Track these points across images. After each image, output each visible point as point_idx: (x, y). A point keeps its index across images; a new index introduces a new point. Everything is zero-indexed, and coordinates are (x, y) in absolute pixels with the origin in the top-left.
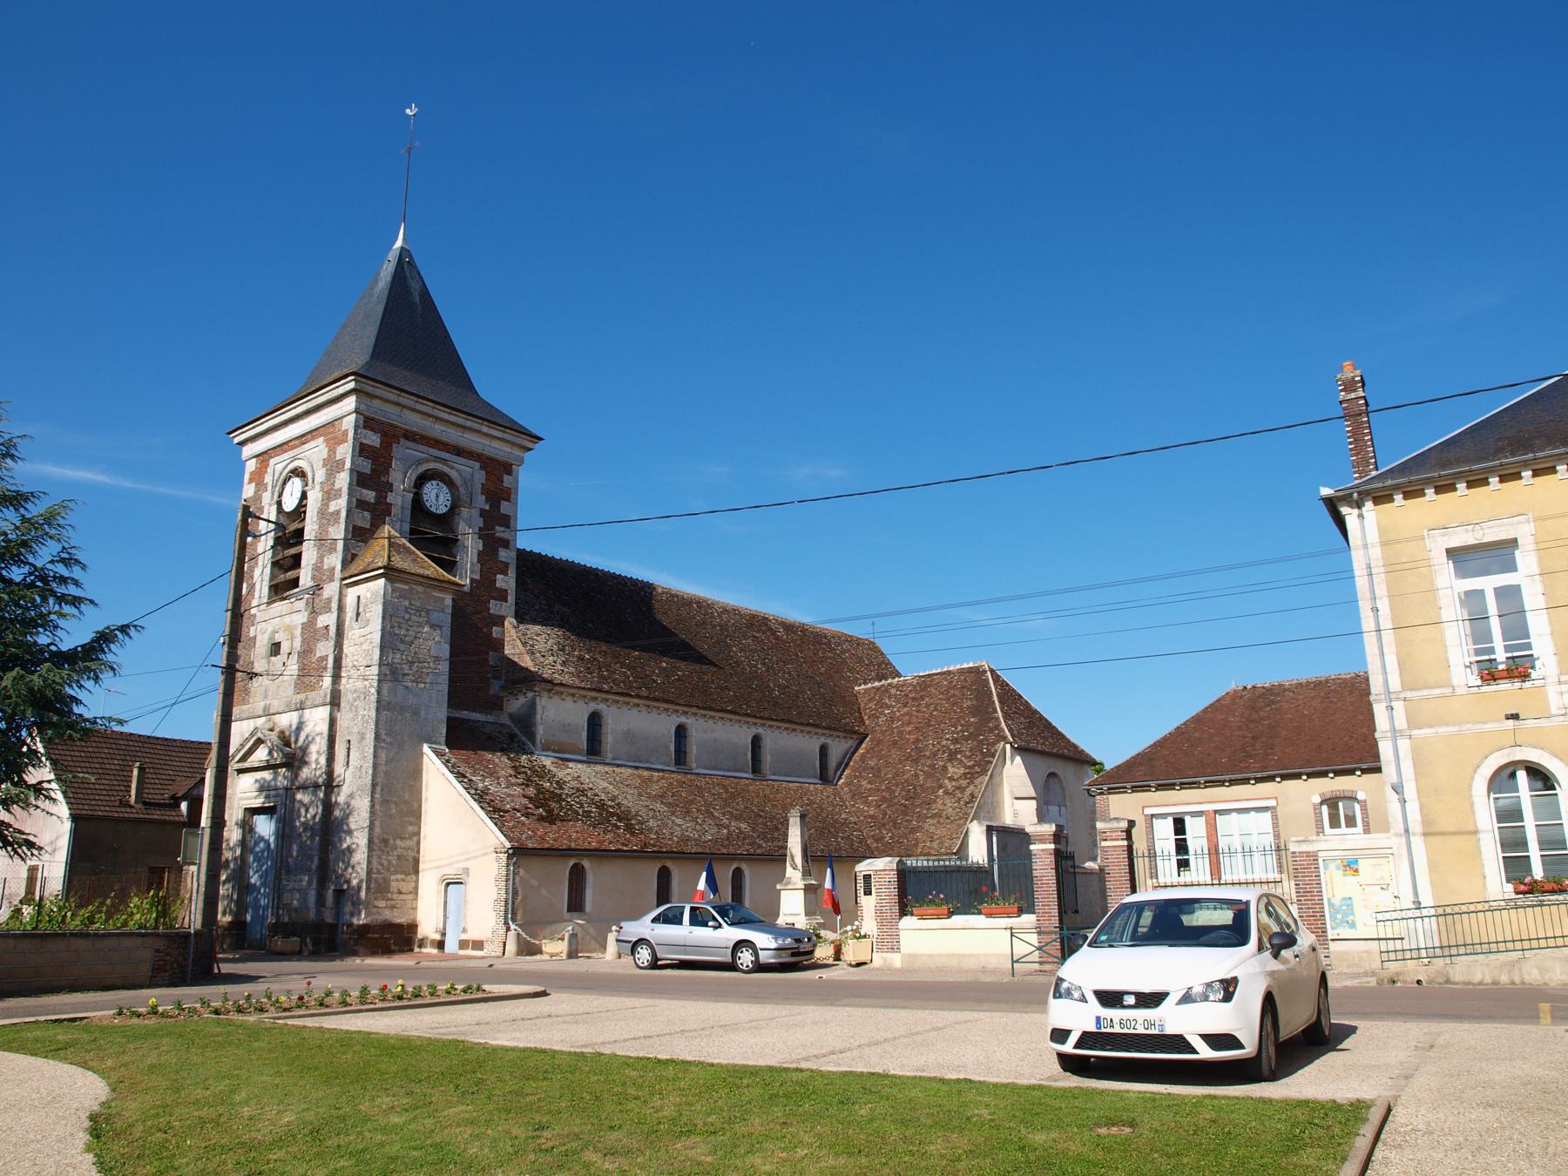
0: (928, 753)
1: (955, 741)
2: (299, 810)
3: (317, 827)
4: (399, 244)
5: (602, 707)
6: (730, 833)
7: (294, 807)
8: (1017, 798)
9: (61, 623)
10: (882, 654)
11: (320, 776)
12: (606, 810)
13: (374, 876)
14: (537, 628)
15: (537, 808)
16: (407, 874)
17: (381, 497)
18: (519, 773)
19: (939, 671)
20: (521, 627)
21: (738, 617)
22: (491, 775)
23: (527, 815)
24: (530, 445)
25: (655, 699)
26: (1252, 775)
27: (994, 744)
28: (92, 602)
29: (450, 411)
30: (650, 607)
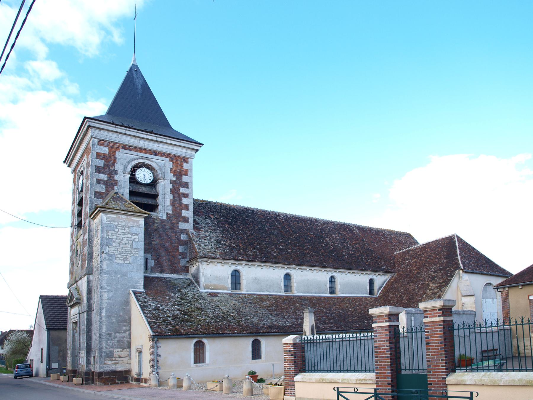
1: (435, 272)
5: (239, 268)
13: (104, 350)
29: (146, 133)
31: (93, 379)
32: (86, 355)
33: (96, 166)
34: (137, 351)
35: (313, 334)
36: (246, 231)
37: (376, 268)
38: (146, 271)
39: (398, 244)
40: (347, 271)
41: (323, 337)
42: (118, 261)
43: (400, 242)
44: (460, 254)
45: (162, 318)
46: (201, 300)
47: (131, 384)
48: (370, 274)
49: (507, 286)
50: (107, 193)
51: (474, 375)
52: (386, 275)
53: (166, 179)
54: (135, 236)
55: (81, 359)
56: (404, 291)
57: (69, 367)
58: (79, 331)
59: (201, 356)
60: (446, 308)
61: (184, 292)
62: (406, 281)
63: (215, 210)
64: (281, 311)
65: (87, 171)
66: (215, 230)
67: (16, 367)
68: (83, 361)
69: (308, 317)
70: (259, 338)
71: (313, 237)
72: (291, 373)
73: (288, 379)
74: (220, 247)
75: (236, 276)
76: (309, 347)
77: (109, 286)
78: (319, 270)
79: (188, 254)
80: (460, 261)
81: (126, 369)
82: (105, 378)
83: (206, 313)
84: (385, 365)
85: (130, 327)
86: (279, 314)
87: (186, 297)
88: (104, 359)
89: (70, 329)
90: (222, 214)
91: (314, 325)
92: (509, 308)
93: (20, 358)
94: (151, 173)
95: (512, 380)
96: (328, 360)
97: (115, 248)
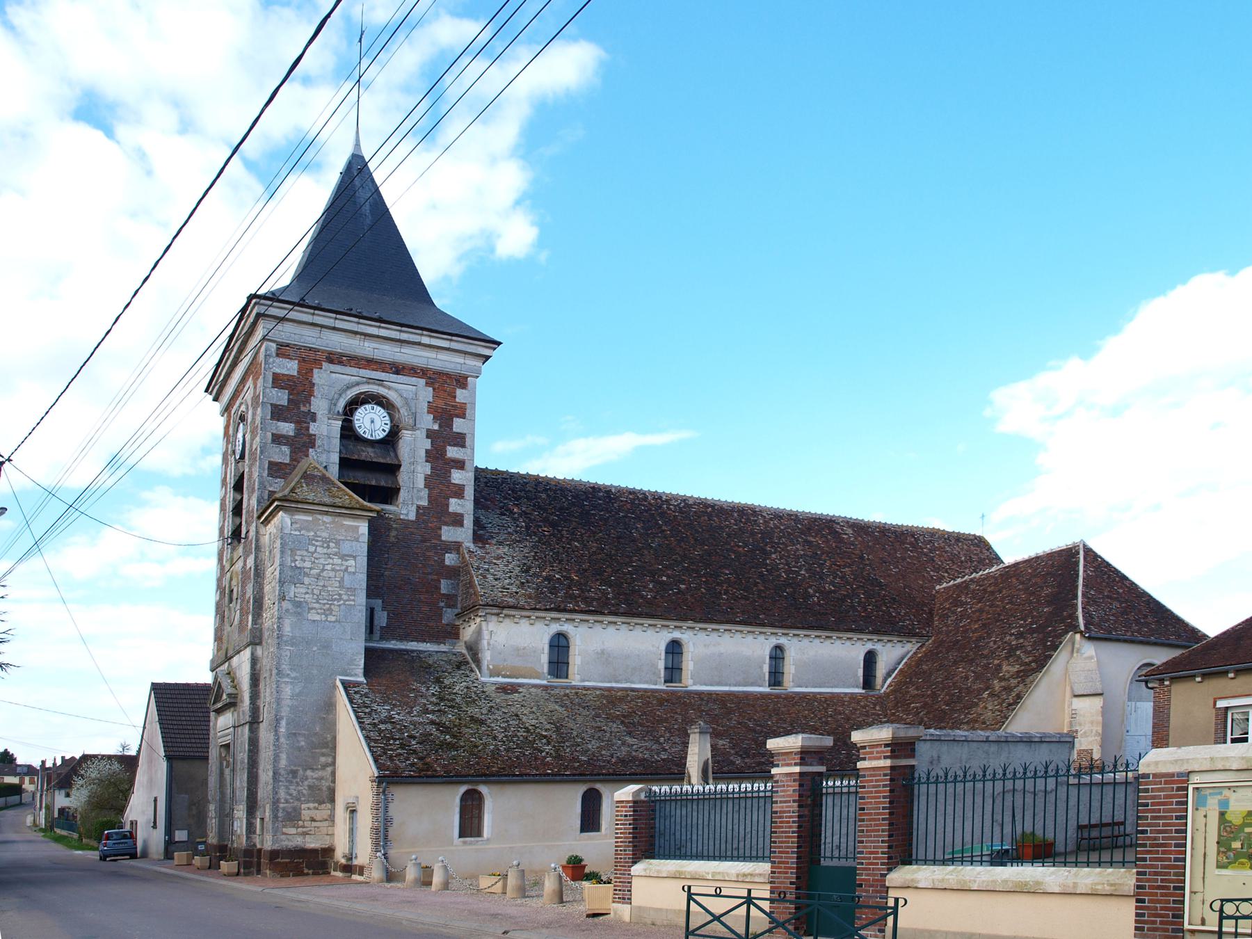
0: (985, 652)
1: (1020, 635)
5: (567, 628)
8: (1076, 696)
13: (281, 805)
24: (486, 352)
31: (259, 864)
32: (247, 815)
33: (271, 404)
34: (348, 808)
35: (705, 780)
36: (588, 542)
37: (885, 627)
38: (370, 637)
39: (948, 565)
40: (814, 633)
41: (734, 789)
42: (313, 616)
43: (953, 558)
44: (1083, 594)
45: (398, 739)
46: (481, 700)
47: (333, 876)
48: (868, 640)
49: (1199, 673)
50: (294, 465)
51: (935, 871)
52: (908, 642)
53: (418, 429)
54: (349, 560)
55: (235, 823)
56: (943, 681)
57: (212, 839)
58: (234, 764)
59: (476, 821)
60: (900, 741)
61: (447, 682)
62: (951, 657)
63: (523, 492)
64: (652, 727)
65: (254, 414)
66: (519, 541)
67: (104, 837)
68: (241, 827)
69: (697, 744)
70: (598, 786)
71: (743, 552)
72: (1161, 923)
73: (621, 870)
74: (528, 582)
75: (560, 646)
76: (673, 808)
77: (295, 670)
78: (748, 632)
79: (460, 599)
80: (1080, 610)
81: (323, 846)
82: (283, 863)
83: (489, 729)
84: (788, 847)
85: (334, 758)
86: (648, 732)
87: (450, 694)
88: (281, 823)
89: (215, 759)
90: (539, 503)
91: (710, 761)
92: (1169, 727)
93: (110, 816)
94: (385, 414)
95: (992, 881)
96: (761, 833)
97: (308, 589)
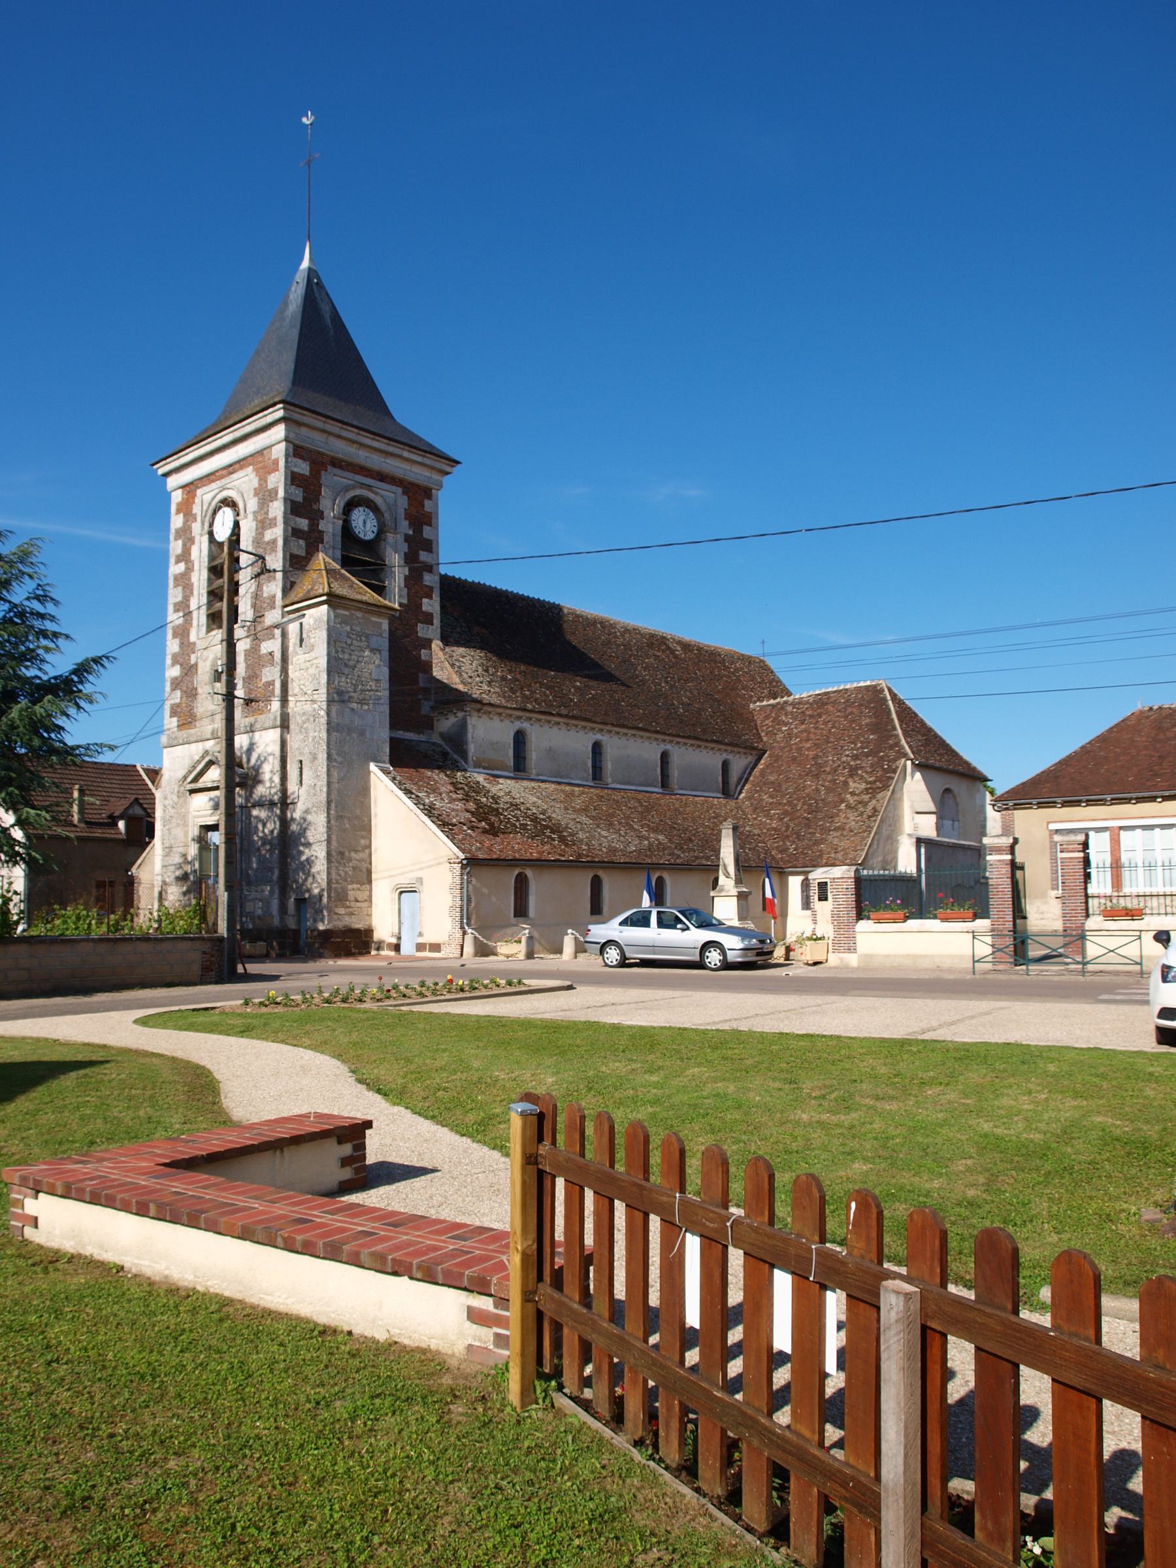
1: (855, 757)
2: (256, 827)
3: (276, 842)
4: (305, 264)
5: (525, 725)
6: (650, 844)
7: (250, 823)
9: (48, 657)
10: (772, 672)
11: (276, 793)
12: (540, 823)
13: (333, 886)
14: (461, 650)
15: (480, 821)
16: (363, 884)
17: (314, 525)
18: (458, 789)
19: (835, 689)
20: (447, 649)
21: (638, 636)
22: (434, 791)
23: (472, 828)
24: (448, 469)
25: (574, 717)
26: (1159, 793)
27: (895, 760)
28: (67, 637)
30: (560, 628)
